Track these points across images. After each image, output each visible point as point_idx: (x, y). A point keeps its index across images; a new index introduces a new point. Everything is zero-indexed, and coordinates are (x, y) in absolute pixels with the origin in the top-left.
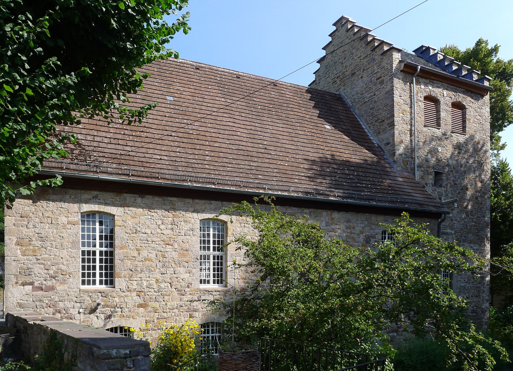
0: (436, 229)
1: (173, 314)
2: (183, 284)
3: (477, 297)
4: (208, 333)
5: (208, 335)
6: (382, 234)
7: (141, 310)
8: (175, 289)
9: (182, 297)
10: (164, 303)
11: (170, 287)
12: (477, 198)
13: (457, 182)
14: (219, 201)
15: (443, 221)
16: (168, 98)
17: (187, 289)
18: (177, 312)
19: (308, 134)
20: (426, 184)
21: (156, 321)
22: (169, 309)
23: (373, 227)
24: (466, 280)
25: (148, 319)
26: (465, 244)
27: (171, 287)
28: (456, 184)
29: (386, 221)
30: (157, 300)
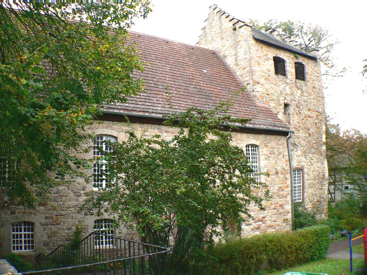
0: (286, 143)
1: (70, 212)
2: (79, 187)
3: (320, 189)
4: (21, 231)
5: (25, 233)
6: (246, 147)
7: (42, 208)
8: (72, 191)
9: (78, 198)
10: (61, 203)
11: (67, 190)
12: (316, 124)
13: (301, 112)
14: (111, 121)
15: (289, 138)
16: (204, 71)
17: (82, 192)
18: (74, 211)
19: (189, 75)
20: (278, 112)
21: (54, 217)
22: (66, 207)
23: (239, 142)
24: (313, 178)
25: (47, 215)
26: (310, 154)
27: (68, 189)
28: (300, 113)
29: (249, 137)
30: (56, 200)
